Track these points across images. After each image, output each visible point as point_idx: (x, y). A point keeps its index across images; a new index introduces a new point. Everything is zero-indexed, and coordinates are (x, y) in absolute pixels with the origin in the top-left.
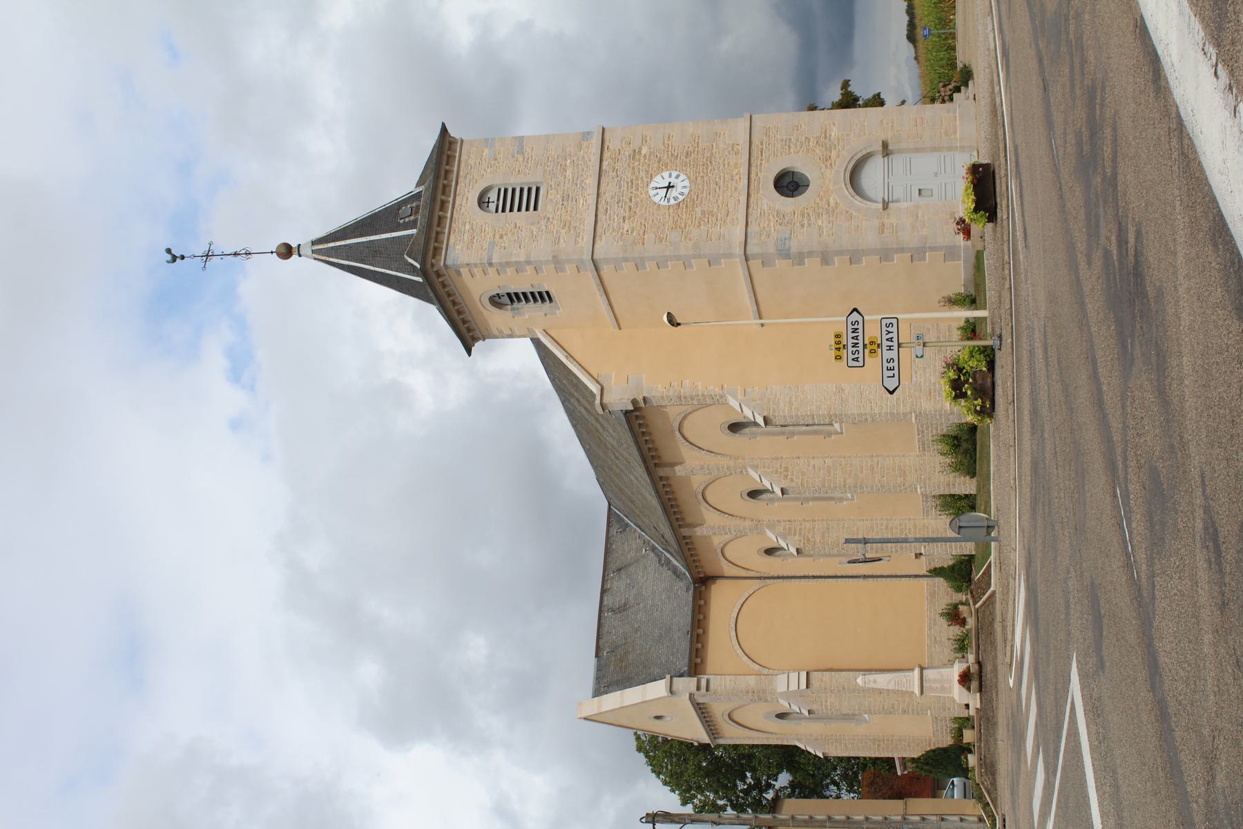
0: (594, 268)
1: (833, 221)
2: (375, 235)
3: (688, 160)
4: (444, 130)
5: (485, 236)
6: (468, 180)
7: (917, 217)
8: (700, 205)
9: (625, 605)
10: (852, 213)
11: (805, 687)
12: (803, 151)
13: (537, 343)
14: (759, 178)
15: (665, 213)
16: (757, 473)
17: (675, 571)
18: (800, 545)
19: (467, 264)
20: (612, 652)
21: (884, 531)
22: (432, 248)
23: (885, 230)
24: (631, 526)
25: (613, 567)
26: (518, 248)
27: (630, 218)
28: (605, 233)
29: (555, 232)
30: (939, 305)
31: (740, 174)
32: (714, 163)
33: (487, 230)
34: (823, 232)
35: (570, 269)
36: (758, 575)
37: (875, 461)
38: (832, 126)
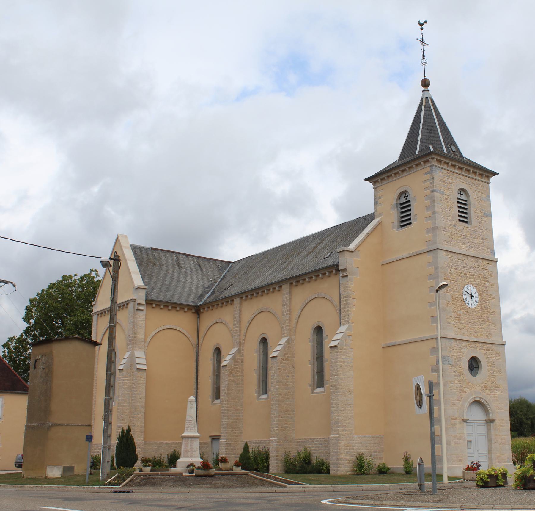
0: (429, 250)
1: (457, 390)
2: (441, 131)
3: (483, 308)
4: (495, 174)
5: (446, 190)
6: (472, 184)
7: (460, 439)
8: (463, 313)
9: (181, 267)
10: (461, 401)
11: (138, 368)
12: (489, 374)
13: (369, 218)
14: (476, 348)
15: (459, 293)
16: (286, 342)
17: (202, 296)
18: (229, 367)
19: (433, 178)
20: (155, 257)
21: (235, 418)
22: (442, 159)
23: (453, 420)
24: (223, 273)
25: (200, 261)
26: (441, 208)
27: (457, 272)
28: (449, 257)
29: (449, 229)
30: (405, 452)
31: (478, 337)
32: (482, 322)
33: (449, 191)
34: (452, 384)
35: (429, 236)
36: (200, 344)
37: (290, 413)
38: (501, 391)
